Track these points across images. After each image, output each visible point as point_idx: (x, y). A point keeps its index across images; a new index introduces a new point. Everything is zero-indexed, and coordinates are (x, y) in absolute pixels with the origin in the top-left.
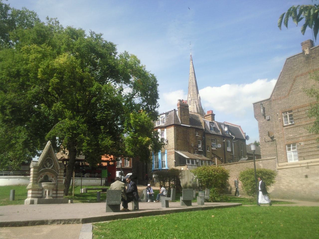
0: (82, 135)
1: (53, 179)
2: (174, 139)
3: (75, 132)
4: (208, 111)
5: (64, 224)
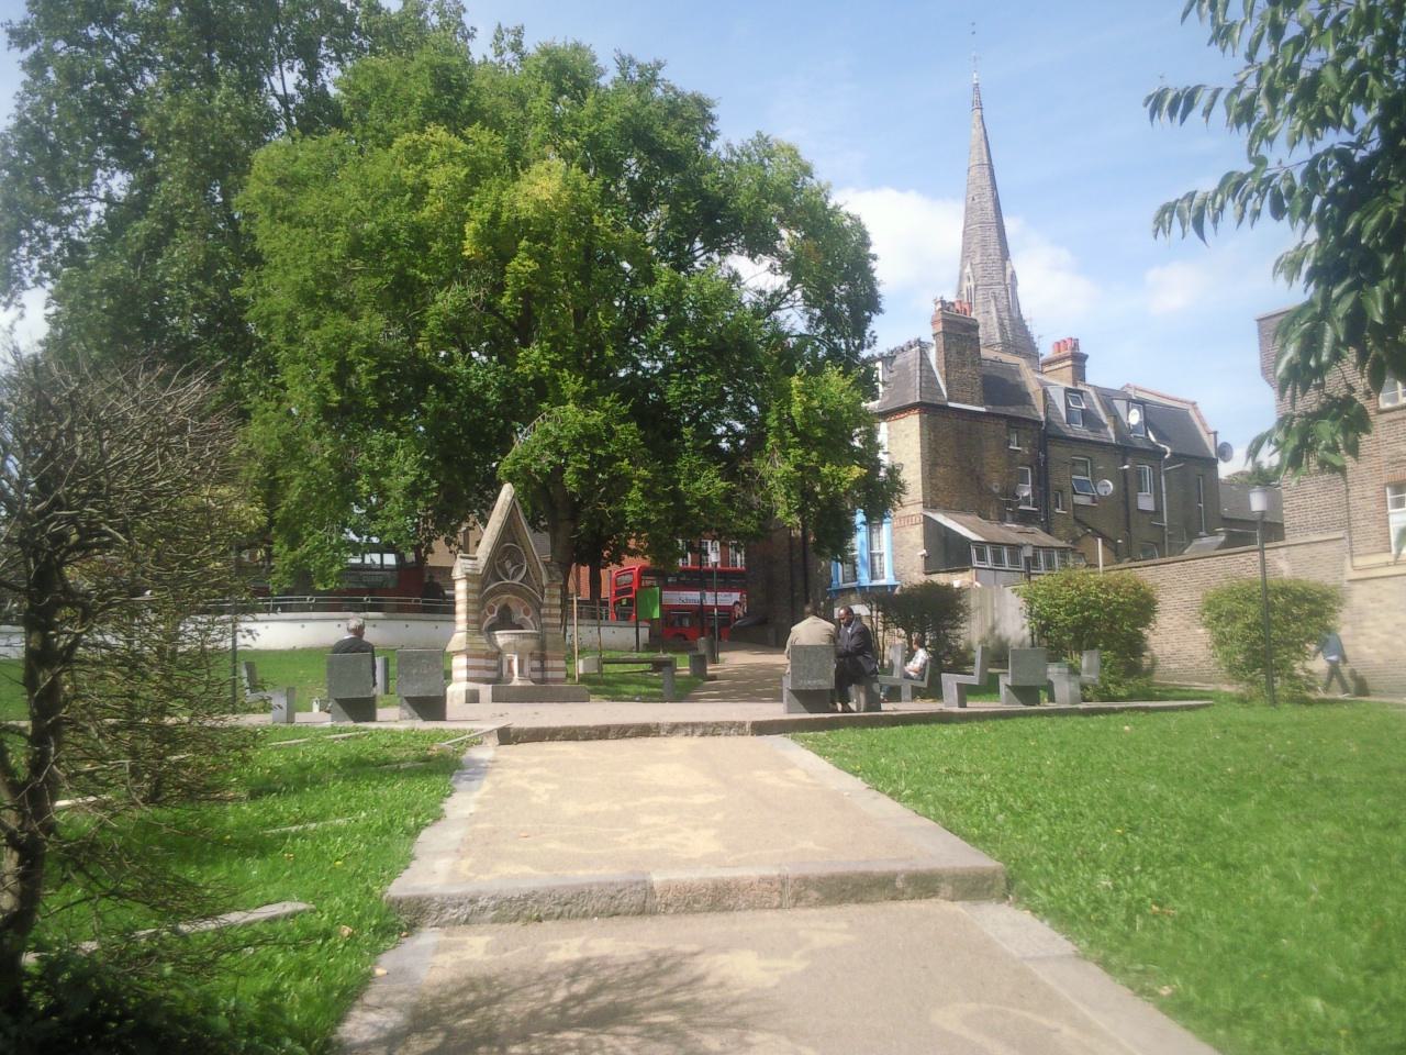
0: (626, 461)
1: (528, 618)
2: (919, 464)
3: (599, 452)
4: (1059, 344)
5: (703, 735)
